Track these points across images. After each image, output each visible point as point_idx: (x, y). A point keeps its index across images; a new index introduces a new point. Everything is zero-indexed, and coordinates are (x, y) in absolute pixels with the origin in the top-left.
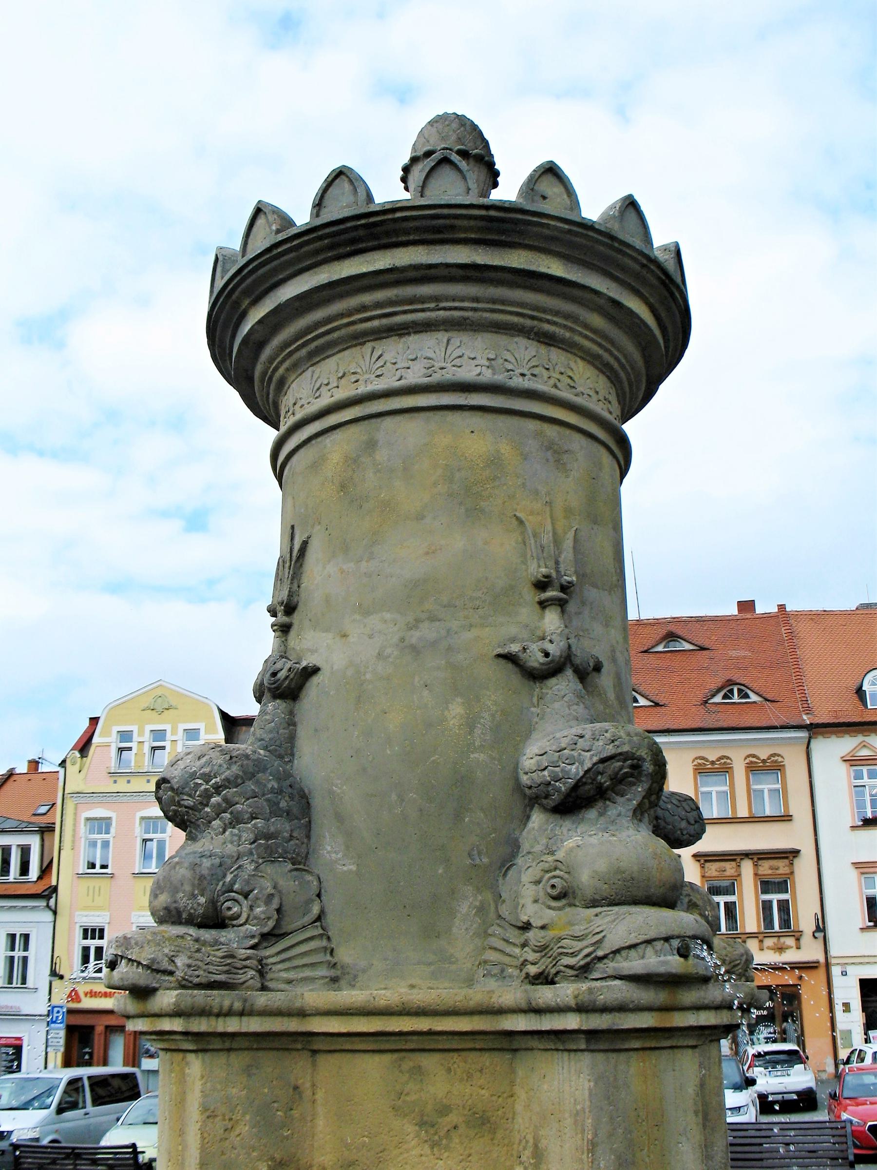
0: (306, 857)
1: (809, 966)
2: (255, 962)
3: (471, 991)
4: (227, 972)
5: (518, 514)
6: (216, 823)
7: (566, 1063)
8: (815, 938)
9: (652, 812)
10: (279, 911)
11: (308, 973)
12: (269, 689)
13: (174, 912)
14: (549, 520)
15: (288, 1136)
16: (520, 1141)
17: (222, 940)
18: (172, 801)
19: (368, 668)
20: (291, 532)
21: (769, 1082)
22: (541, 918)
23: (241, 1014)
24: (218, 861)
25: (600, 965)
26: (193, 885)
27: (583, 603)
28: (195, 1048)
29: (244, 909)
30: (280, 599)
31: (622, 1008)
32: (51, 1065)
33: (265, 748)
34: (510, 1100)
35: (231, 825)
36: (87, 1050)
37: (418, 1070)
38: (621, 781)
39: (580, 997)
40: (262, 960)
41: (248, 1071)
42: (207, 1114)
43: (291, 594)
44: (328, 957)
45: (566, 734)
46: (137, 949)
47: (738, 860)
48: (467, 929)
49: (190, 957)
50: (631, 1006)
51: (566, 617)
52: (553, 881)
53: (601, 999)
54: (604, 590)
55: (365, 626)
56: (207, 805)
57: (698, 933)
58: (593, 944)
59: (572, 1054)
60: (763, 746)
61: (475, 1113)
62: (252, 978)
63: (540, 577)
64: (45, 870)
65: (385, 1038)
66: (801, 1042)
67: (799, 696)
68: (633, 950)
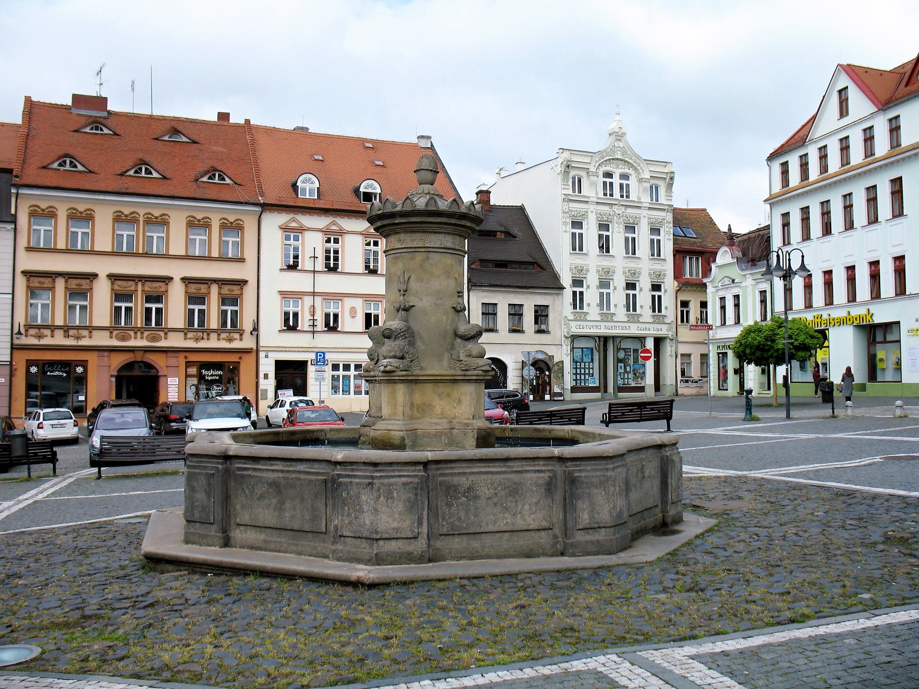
1: (247, 351)
60: (232, 213)
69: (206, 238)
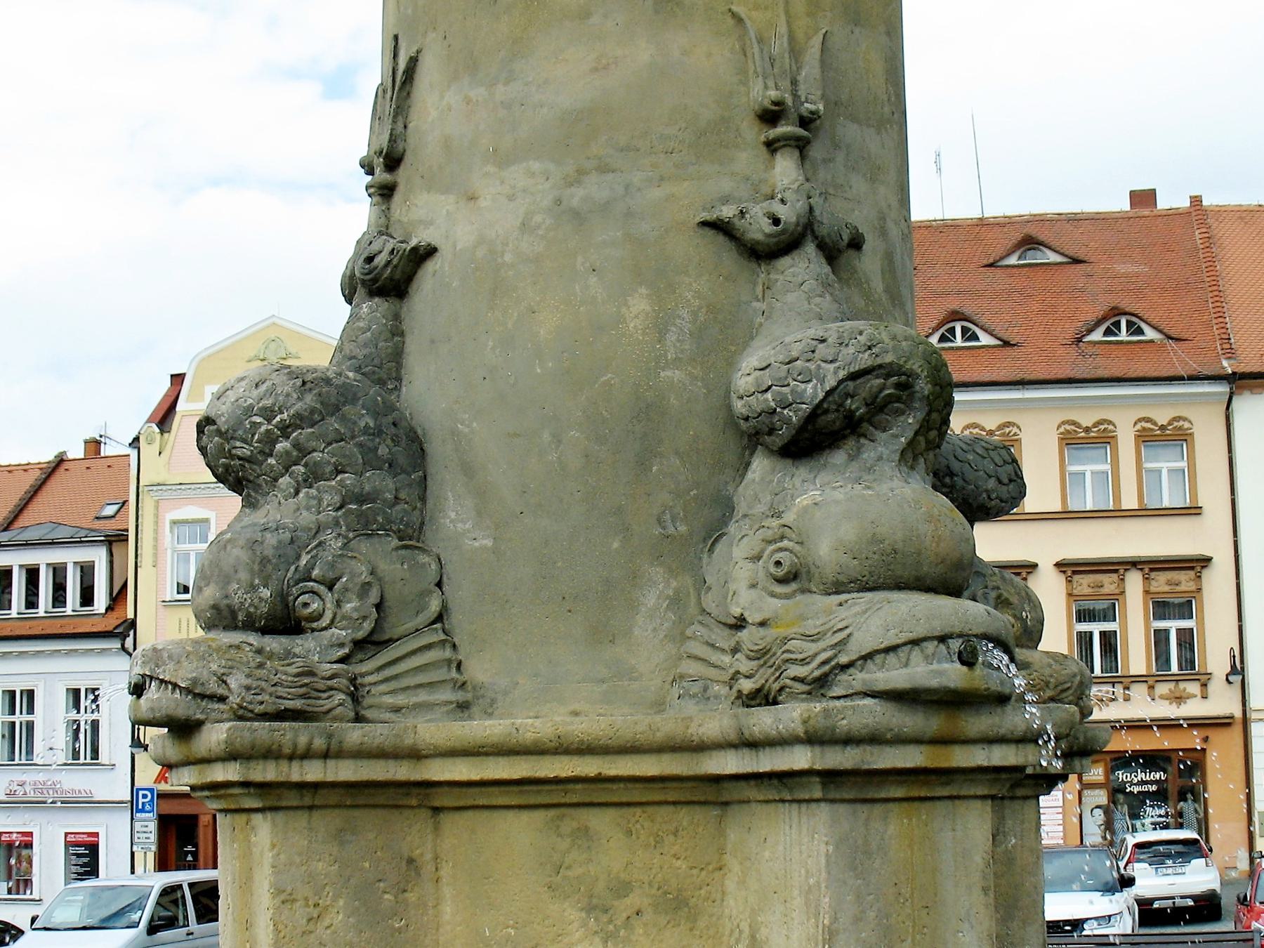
0: (421, 528)
1: (1222, 723)
2: (345, 681)
3: (658, 718)
4: (303, 696)
5: (734, 8)
6: (285, 481)
7: (796, 820)
8: (1230, 683)
9: (931, 455)
10: (379, 607)
11: (422, 696)
12: (363, 282)
13: (226, 613)
14: (783, 18)
15: (400, 928)
16: (732, 931)
17: (297, 650)
18: (221, 452)
19: (507, 244)
20: (394, 45)
21: (1153, 882)
22: (760, 609)
23: (326, 755)
24: (288, 535)
25: (843, 677)
26: (252, 571)
27: (836, 146)
28: (260, 805)
29: (328, 605)
30: (377, 148)
31: (874, 739)
32: (139, 868)
33: (358, 369)
34: (717, 874)
35: (308, 481)
36: (190, 848)
37: (584, 832)
38: (881, 409)
39: (812, 722)
40: (355, 678)
41: (339, 836)
42: (283, 897)
43: (393, 139)
44: (454, 674)
45: (799, 337)
46: (171, 666)
47: (1122, 571)
48: (655, 630)
49: (248, 676)
50: (889, 736)
51: (807, 166)
52: (777, 556)
53: (843, 725)
54: (869, 126)
55: (502, 182)
56: (271, 455)
57: (991, 630)
58: (833, 646)
59: (804, 806)
60: (1162, 404)
61: (666, 893)
62: (340, 705)
63: (767, 104)
64: (117, 598)
65: (534, 788)
66: (1203, 826)
67: (1217, 332)
68: (892, 654)
69: (1107, 467)
